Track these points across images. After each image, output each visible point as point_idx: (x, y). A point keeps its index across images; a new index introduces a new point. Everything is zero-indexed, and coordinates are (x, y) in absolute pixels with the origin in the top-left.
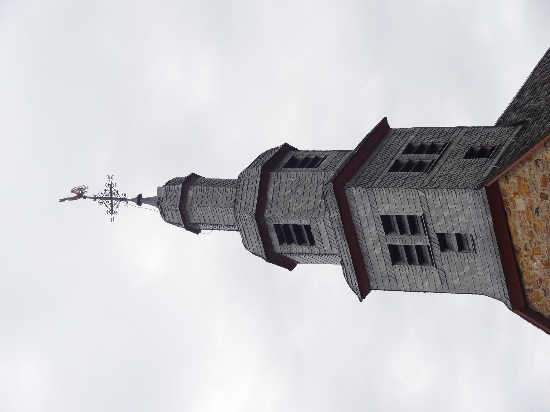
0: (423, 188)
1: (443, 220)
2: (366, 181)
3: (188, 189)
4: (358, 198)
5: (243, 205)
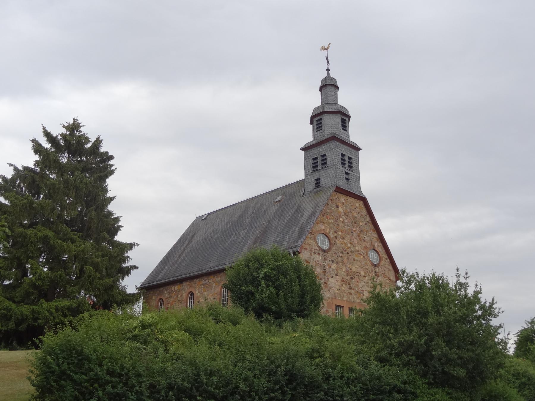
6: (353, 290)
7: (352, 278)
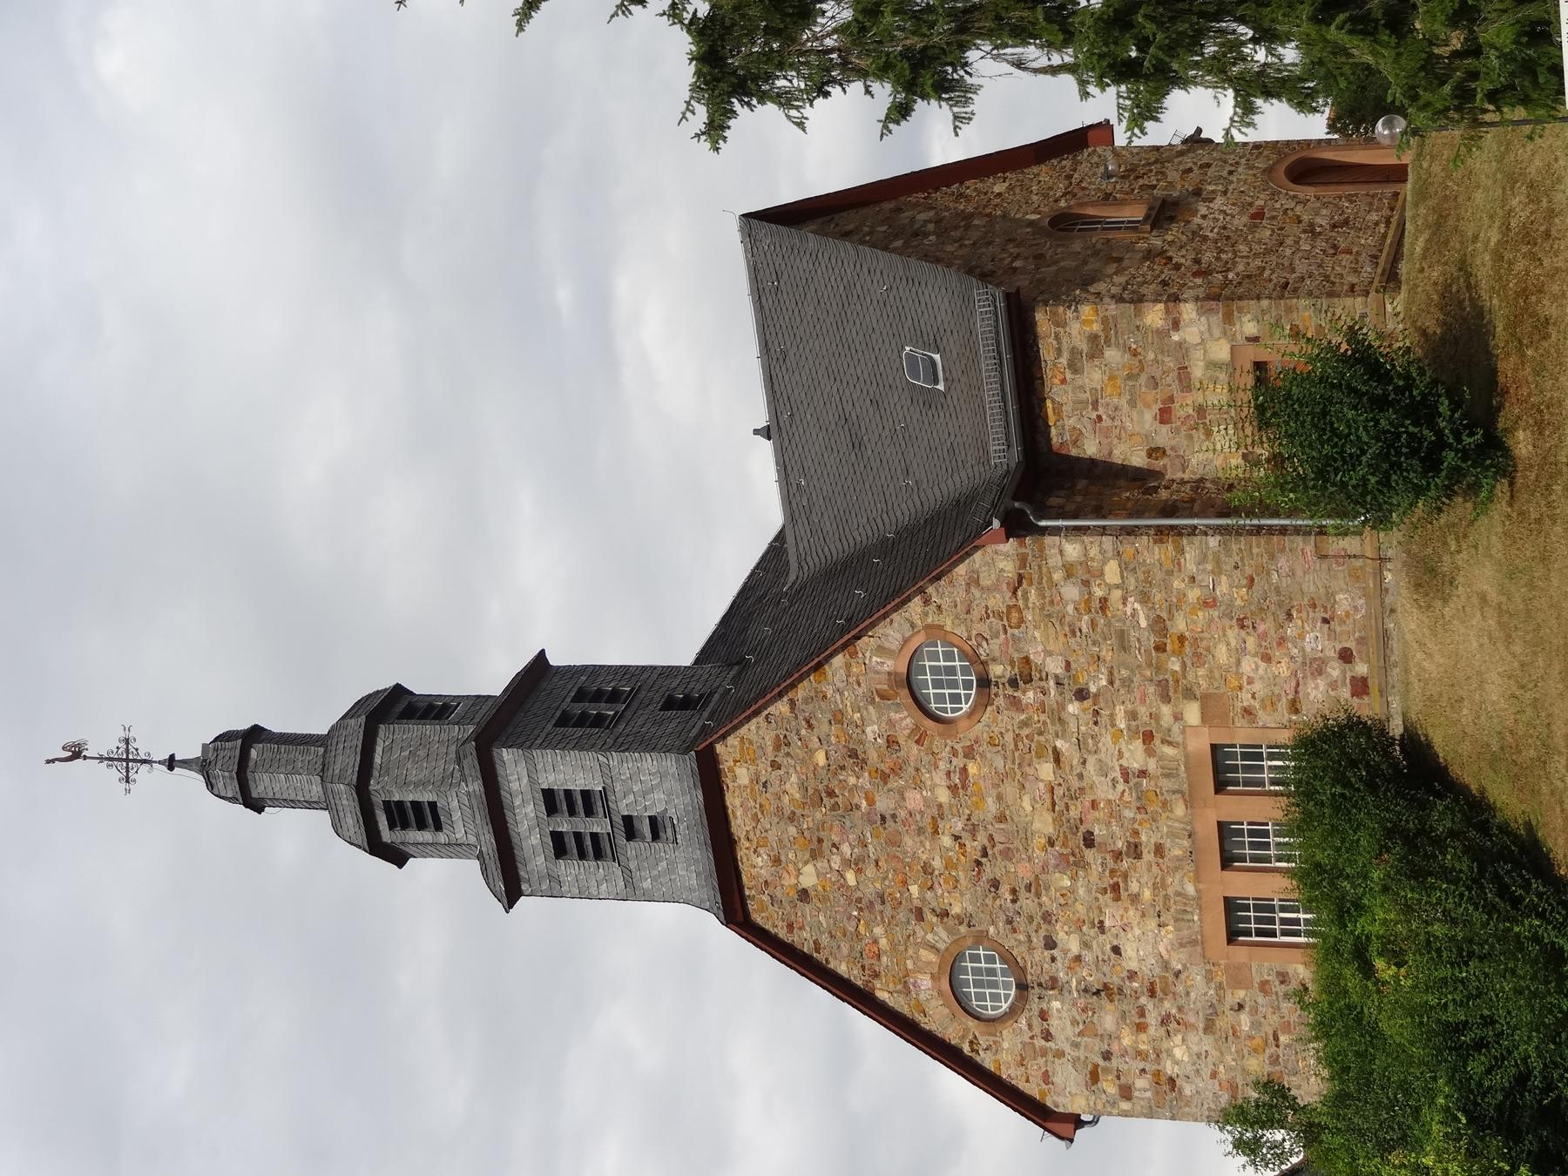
0: (604, 749)
1: (632, 796)
4: (510, 768)
5: (337, 772)
6: (1136, 833)
7: (1089, 841)
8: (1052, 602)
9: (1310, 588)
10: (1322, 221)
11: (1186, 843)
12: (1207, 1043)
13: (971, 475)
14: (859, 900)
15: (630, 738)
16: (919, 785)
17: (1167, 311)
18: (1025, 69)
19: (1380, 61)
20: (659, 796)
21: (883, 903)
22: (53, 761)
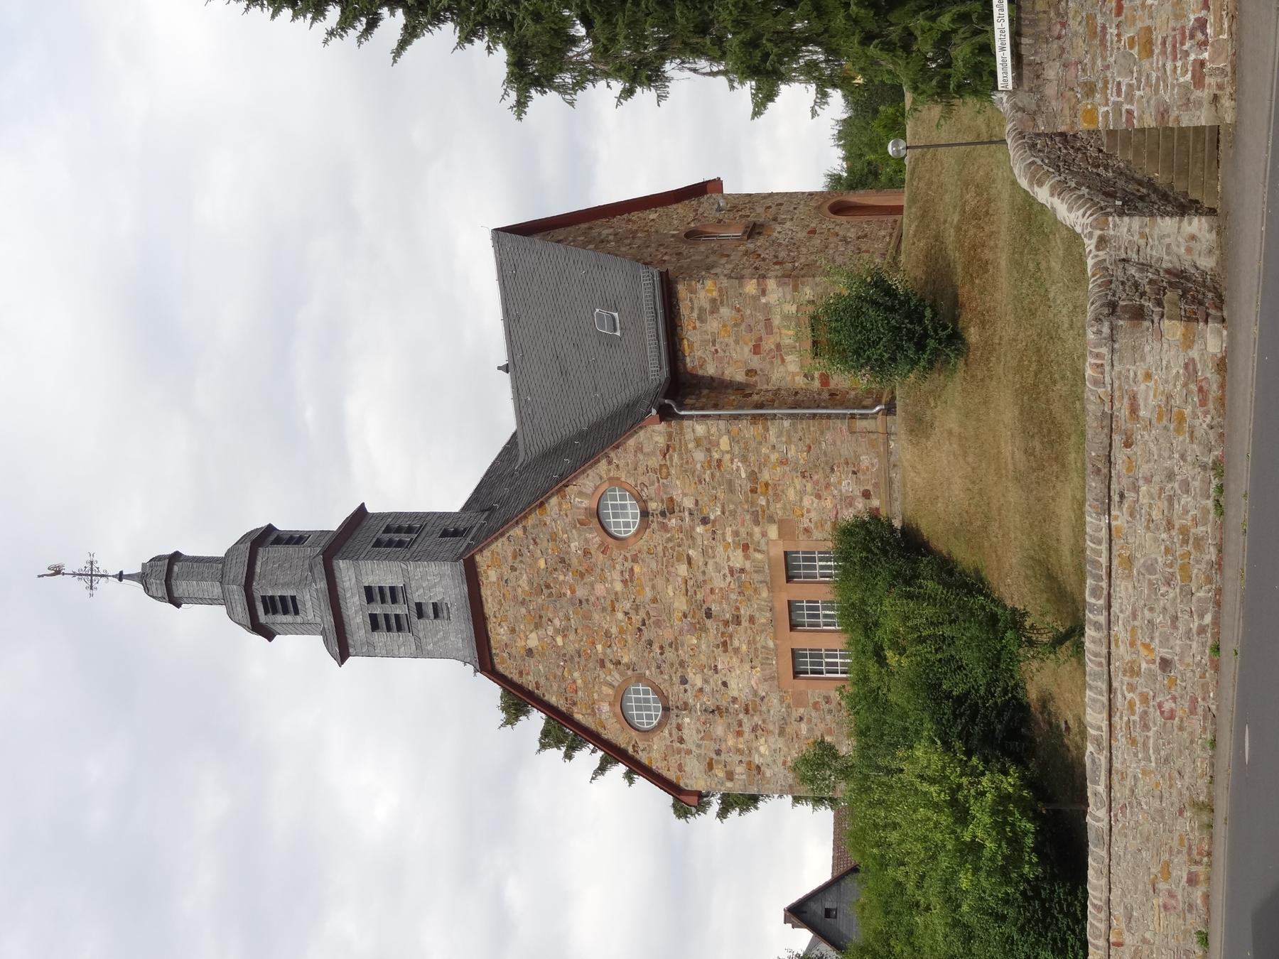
0: (405, 560)
1: (422, 590)
2: (352, 555)
3: (173, 564)
4: (344, 573)
5: (232, 577)
6: (738, 608)
7: (709, 614)
8: (687, 462)
9: (845, 452)
10: (852, 234)
11: (768, 614)
12: (780, 743)
13: (636, 389)
14: (564, 655)
15: (421, 554)
16: (603, 580)
17: (759, 284)
18: (698, 73)
19: (898, 68)
20: (439, 589)
21: (580, 656)
22: (42, 576)
